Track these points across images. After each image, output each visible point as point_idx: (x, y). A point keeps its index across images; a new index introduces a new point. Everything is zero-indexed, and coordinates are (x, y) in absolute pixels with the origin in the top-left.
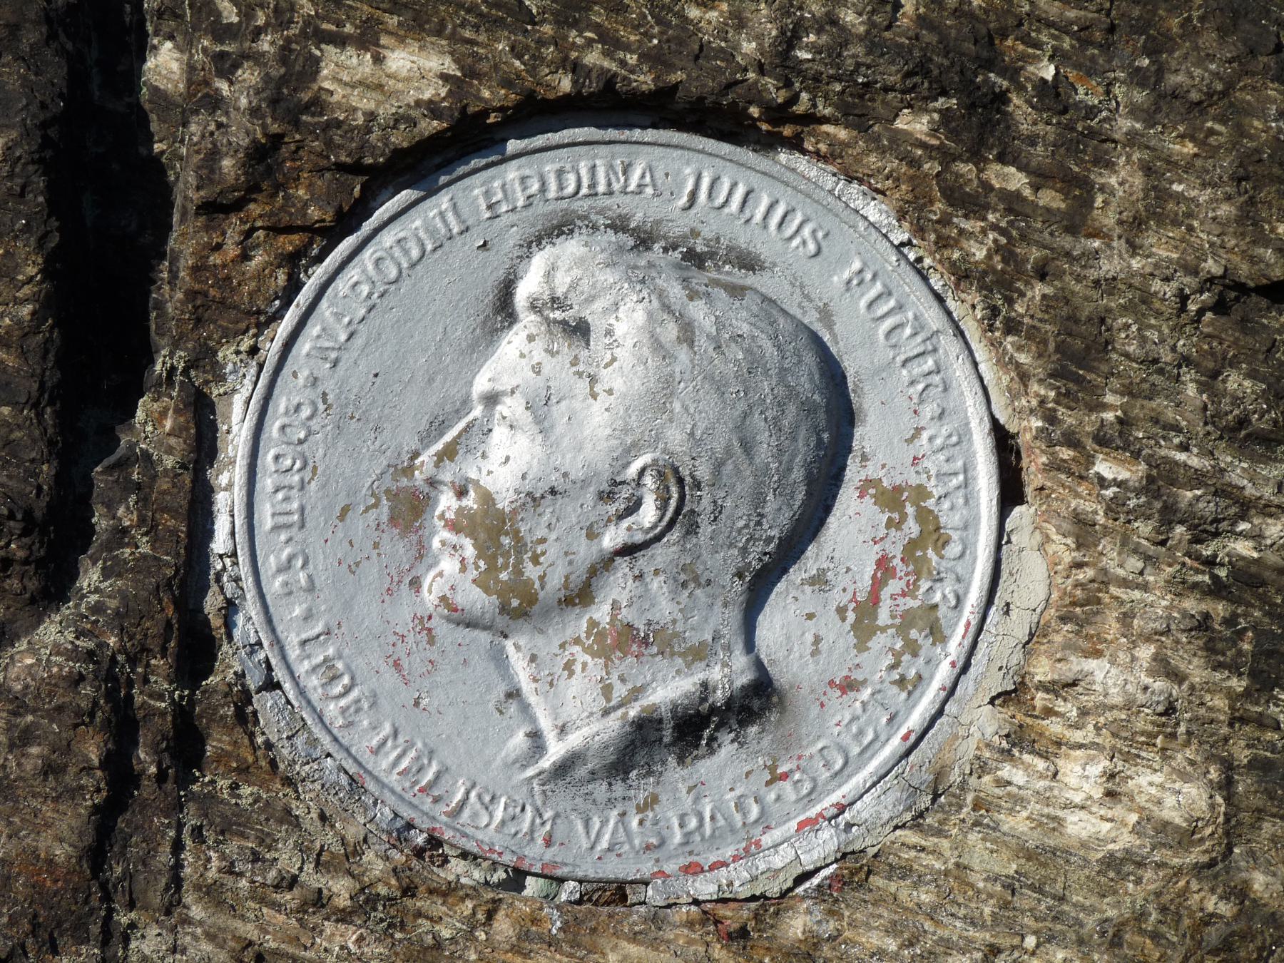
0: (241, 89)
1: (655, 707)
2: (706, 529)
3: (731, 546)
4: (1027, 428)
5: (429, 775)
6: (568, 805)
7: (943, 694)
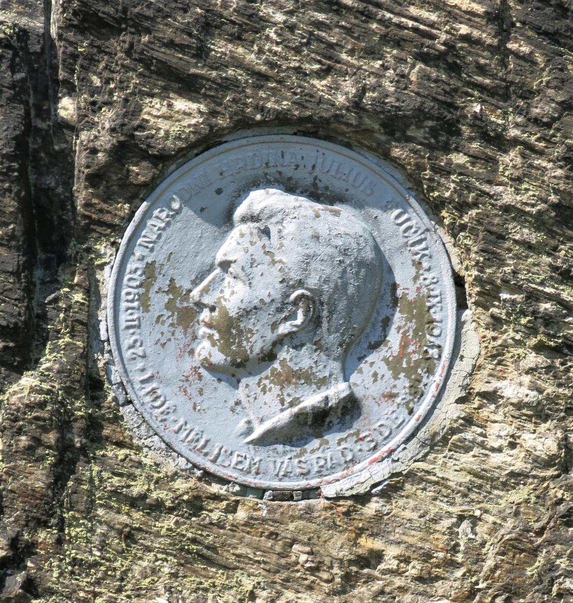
0: (107, 117)
1: (306, 407)
2: (325, 325)
3: (337, 332)
4: (470, 276)
5: (202, 442)
6: (266, 455)
7: (434, 399)
